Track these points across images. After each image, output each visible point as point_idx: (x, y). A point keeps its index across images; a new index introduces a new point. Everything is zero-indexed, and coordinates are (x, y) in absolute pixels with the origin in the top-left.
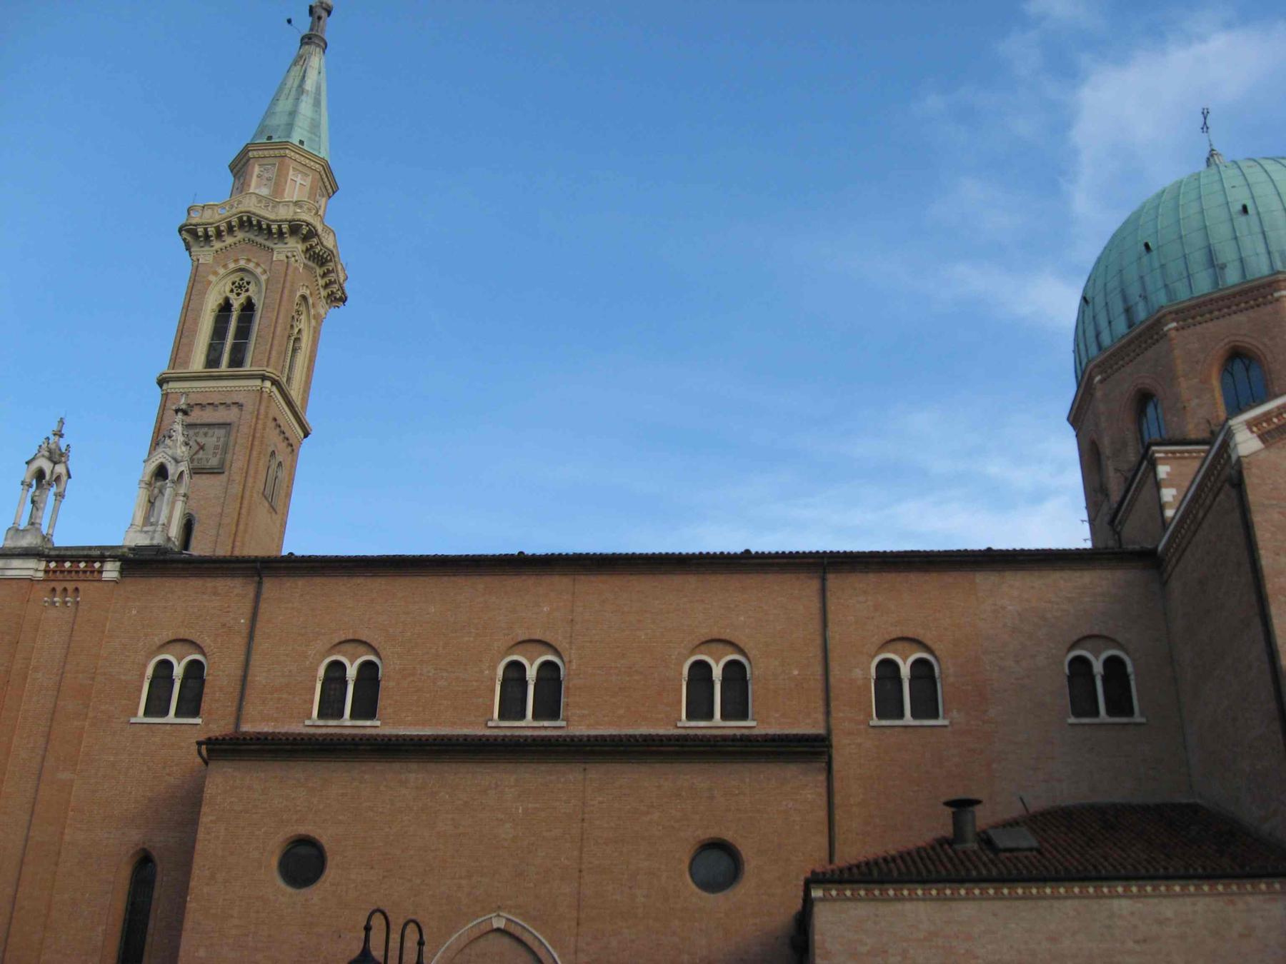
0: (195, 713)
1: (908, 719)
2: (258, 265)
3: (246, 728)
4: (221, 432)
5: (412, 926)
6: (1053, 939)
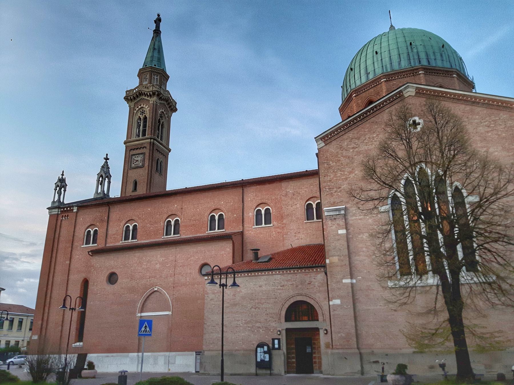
0: (96, 243)
1: (263, 225)
2: (140, 105)
3: (107, 245)
4: (142, 156)
5: (204, 272)
6: (260, 286)
